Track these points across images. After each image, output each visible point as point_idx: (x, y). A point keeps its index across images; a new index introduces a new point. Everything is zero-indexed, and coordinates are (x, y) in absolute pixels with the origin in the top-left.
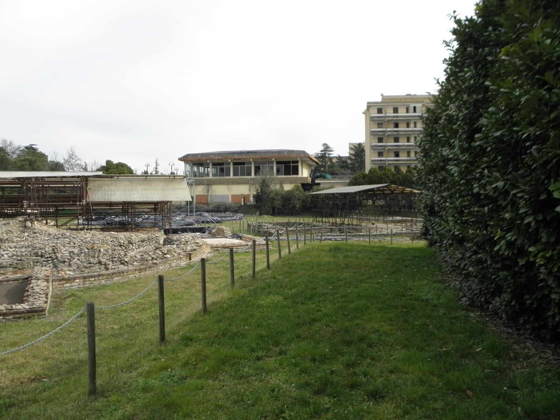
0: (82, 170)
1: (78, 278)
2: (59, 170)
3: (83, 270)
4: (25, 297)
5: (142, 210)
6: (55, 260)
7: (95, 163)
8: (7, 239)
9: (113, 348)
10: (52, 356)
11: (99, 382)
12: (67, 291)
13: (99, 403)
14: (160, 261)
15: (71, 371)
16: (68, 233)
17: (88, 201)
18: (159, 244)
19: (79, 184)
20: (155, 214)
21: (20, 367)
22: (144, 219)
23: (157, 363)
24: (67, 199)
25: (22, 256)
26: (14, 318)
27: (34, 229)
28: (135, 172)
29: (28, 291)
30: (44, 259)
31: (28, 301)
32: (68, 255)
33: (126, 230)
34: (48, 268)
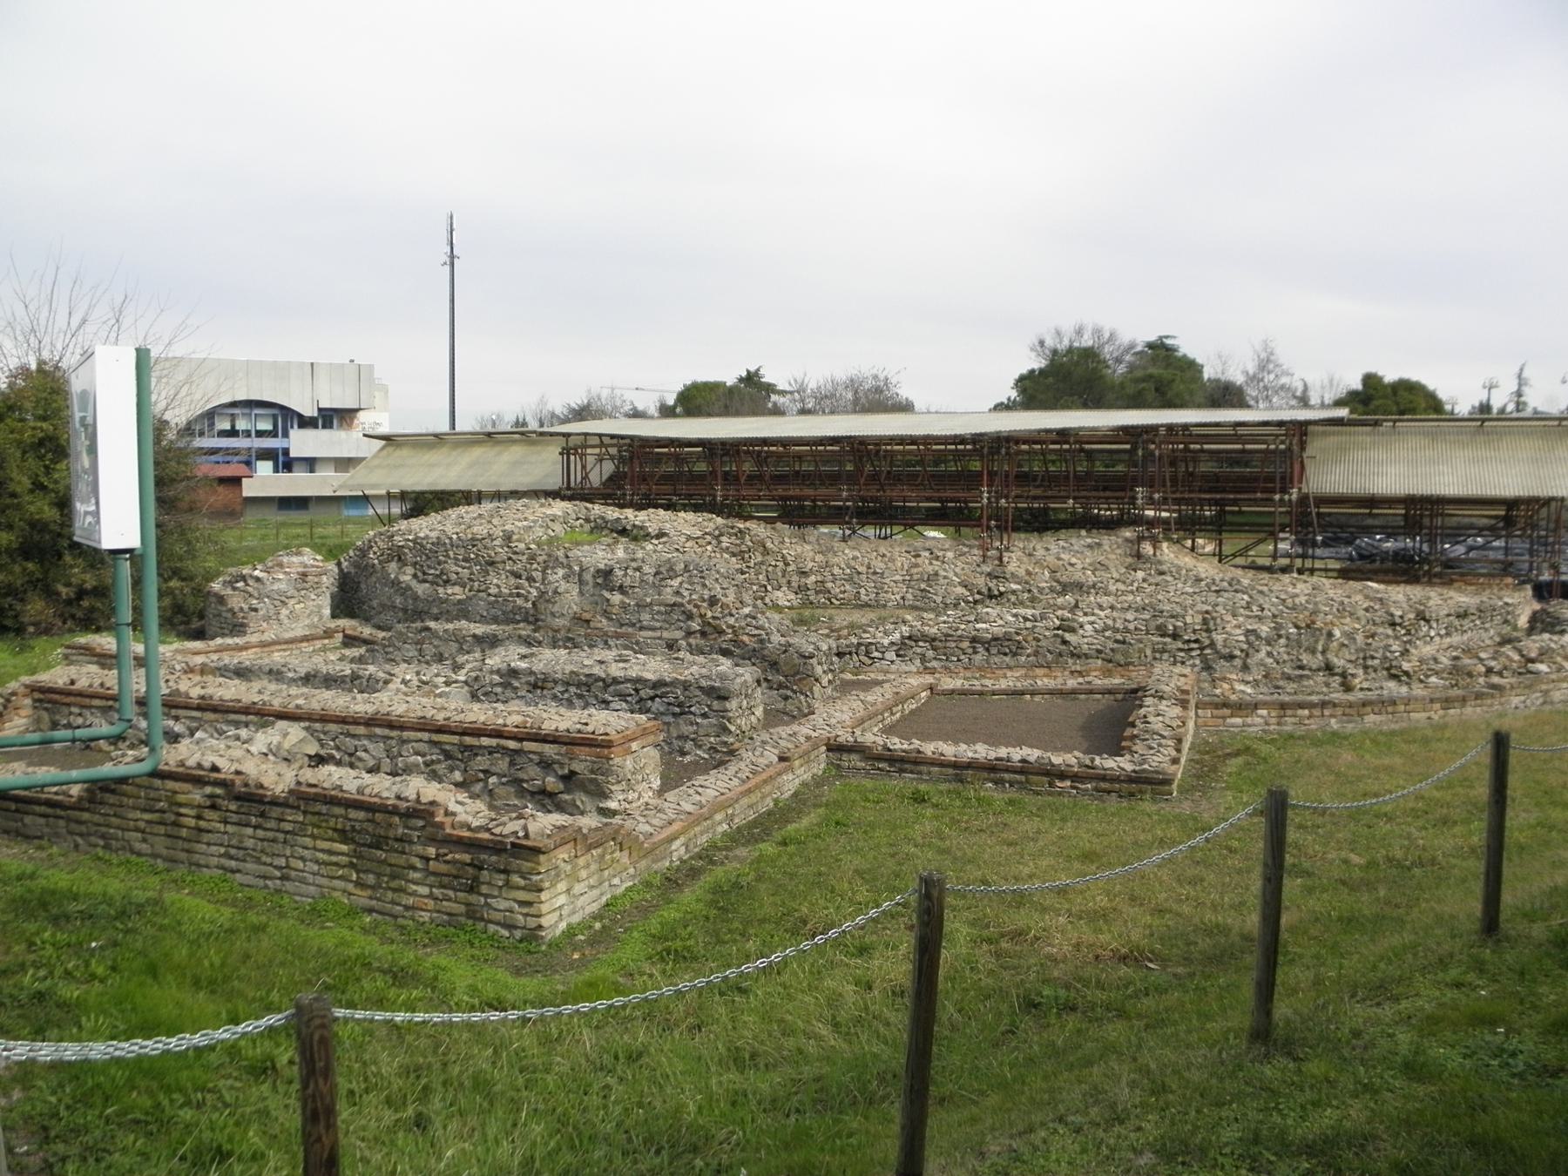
0: (1293, 402)
1: (1265, 705)
2: (1232, 405)
3: (1281, 683)
4: (1125, 739)
5: (1467, 520)
6: (1208, 651)
7: (1331, 381)
8: (1094, 586)
9: (1340, 919)
10: (1175, 907)
11: (1282, 1010)
12: (1233, 736)
13: (1273, 1071)
14: (1513, 680)
15: (1219, 959)
16: (1246, 579)
17: (1305, 490)
18: (1515, 628)
19: (1282, 442)
20: (1508, 536)
21: (1098, 917)
22: (1471, 549)
23: (1464, 1000)
24: (1247, 484)
25: (1128, 631)
26: (1097, 789)
27: (1160, 563)
28: (1448, 407)
29: (1133, 725)
30: (1180, 645)
31: (1132, 752)
32: (1242, 638)
33: (1412, 578)
34: (1187, 671)
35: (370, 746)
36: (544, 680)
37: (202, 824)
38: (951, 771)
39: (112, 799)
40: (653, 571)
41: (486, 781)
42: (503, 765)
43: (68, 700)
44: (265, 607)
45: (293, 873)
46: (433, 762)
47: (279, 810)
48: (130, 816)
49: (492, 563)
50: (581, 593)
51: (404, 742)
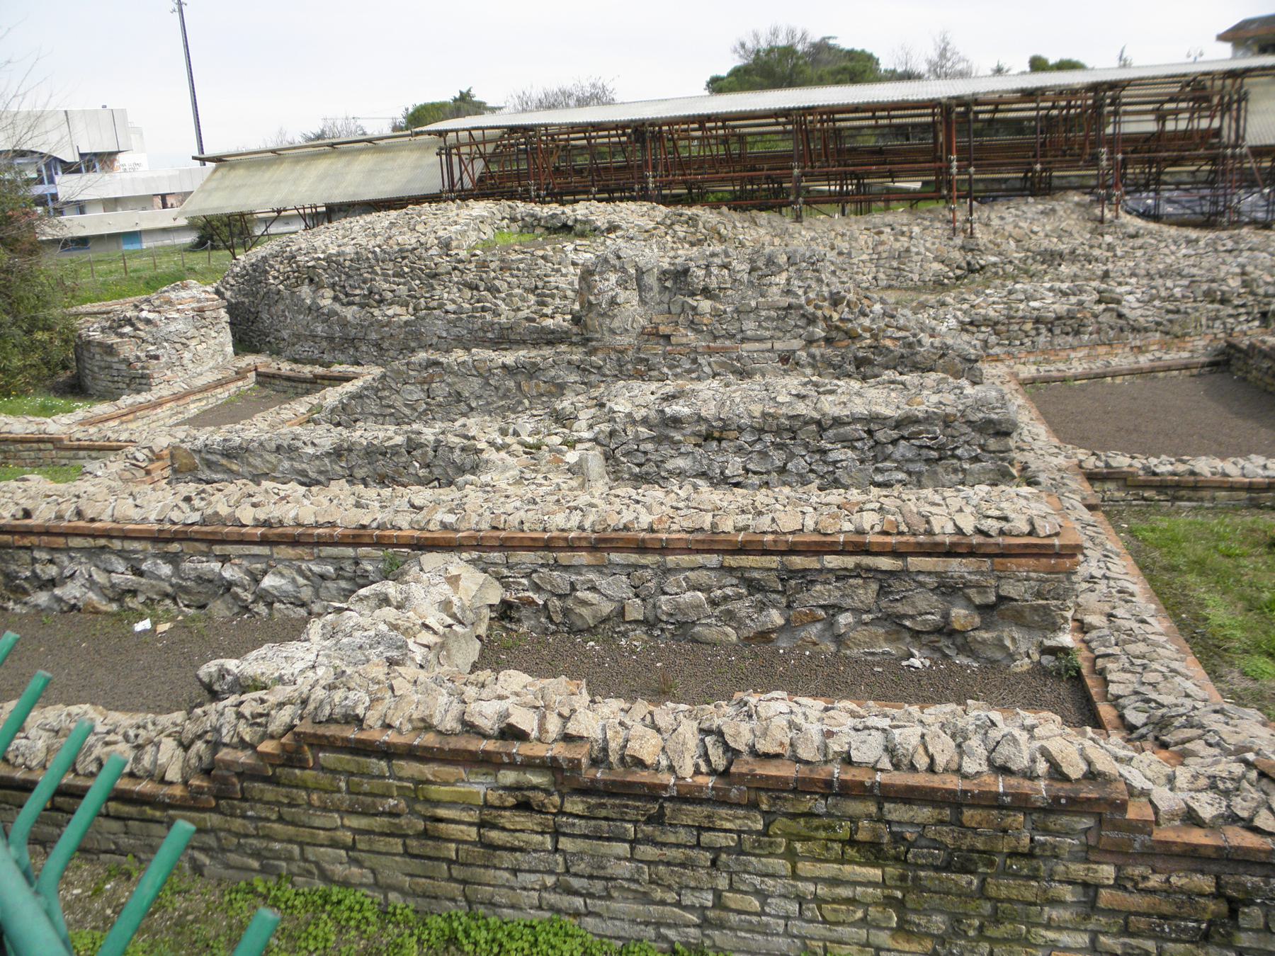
35: (602, 582)
36: (724, 428)
37: (494, 835)
38: (1244, 495)
39: (270, 792)
40: (746, 267)
41: (831, 624)
42: (866, 594)
43: (26, 541)
44: (166, 352)
45: (734, 918)
46: (726, 598)
47: (704, 810)
48: (318, 822)
49: (435, 276)
50: (643, 301)
51: (667, 571)
